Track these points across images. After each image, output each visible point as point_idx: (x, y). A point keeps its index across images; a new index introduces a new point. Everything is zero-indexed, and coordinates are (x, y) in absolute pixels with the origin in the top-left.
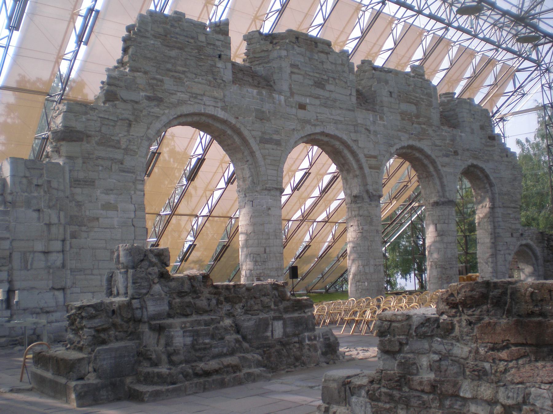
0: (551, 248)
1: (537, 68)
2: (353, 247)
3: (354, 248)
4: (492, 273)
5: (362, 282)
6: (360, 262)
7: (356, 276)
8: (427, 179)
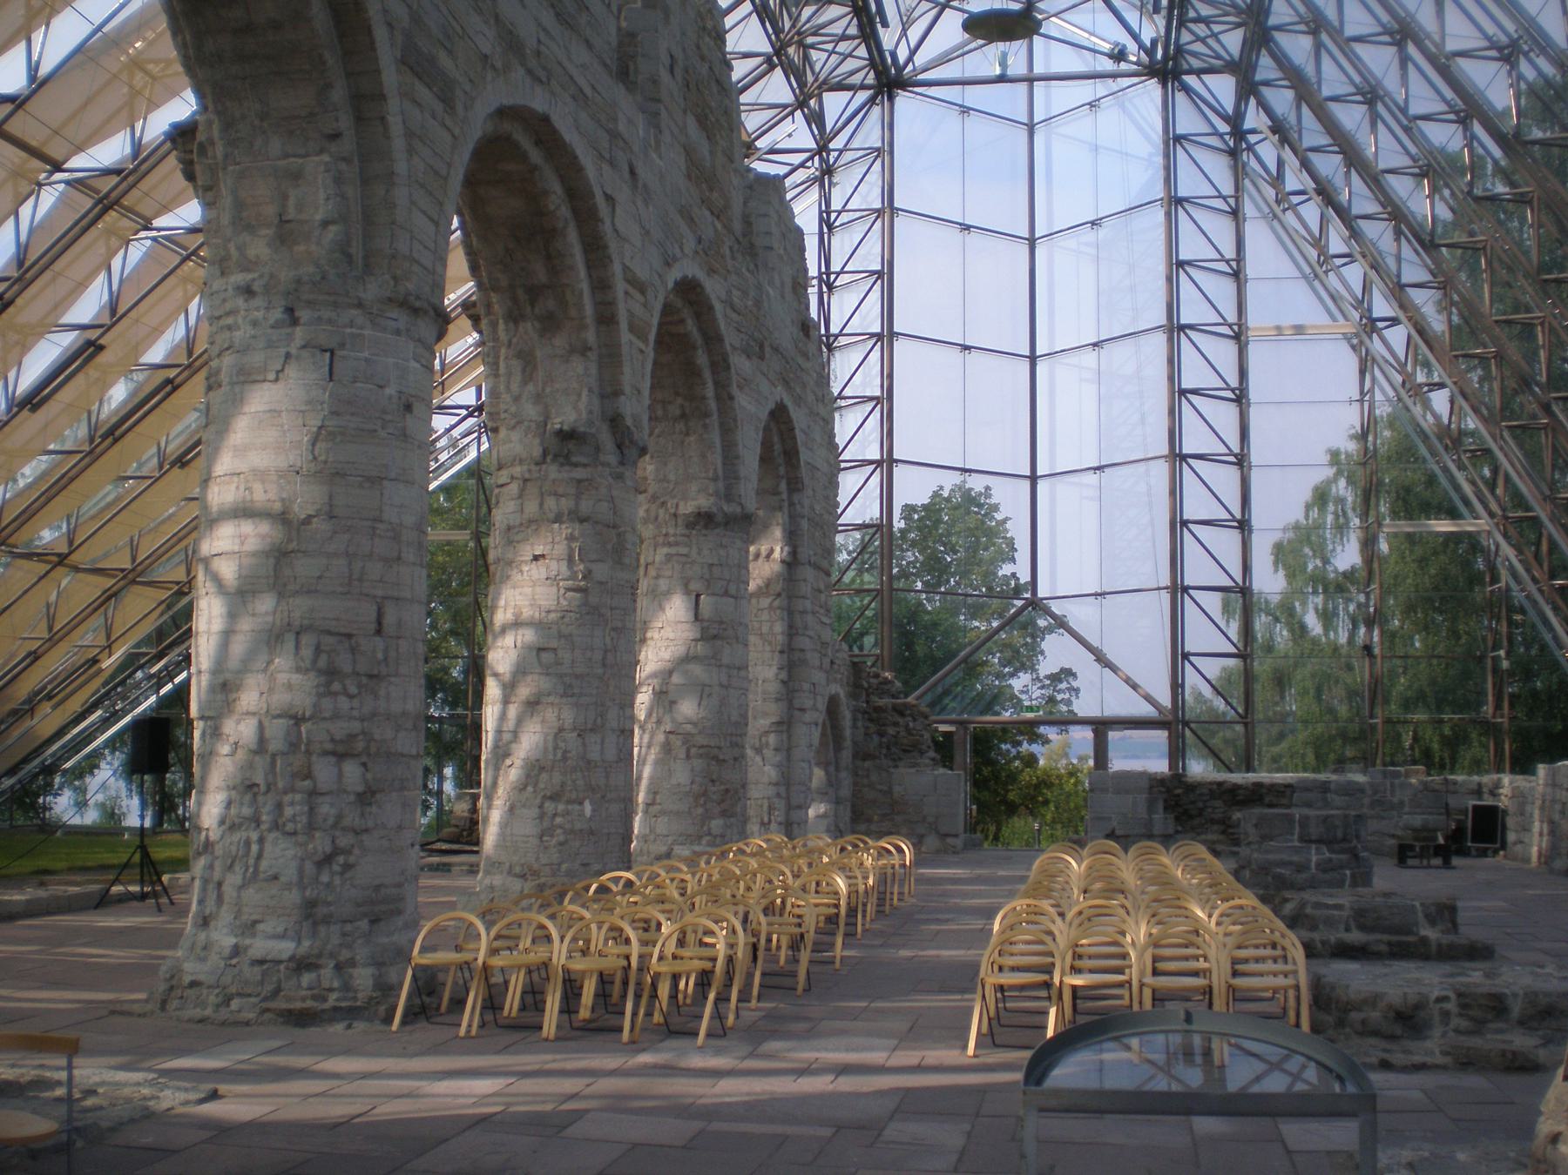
0: (875, 715)
2: (540, 650)
3: (544, 655)
4: (776, 784)
5: (569, 802)
6: (568, 716)
7: (544, 776)
8: (680, 426)
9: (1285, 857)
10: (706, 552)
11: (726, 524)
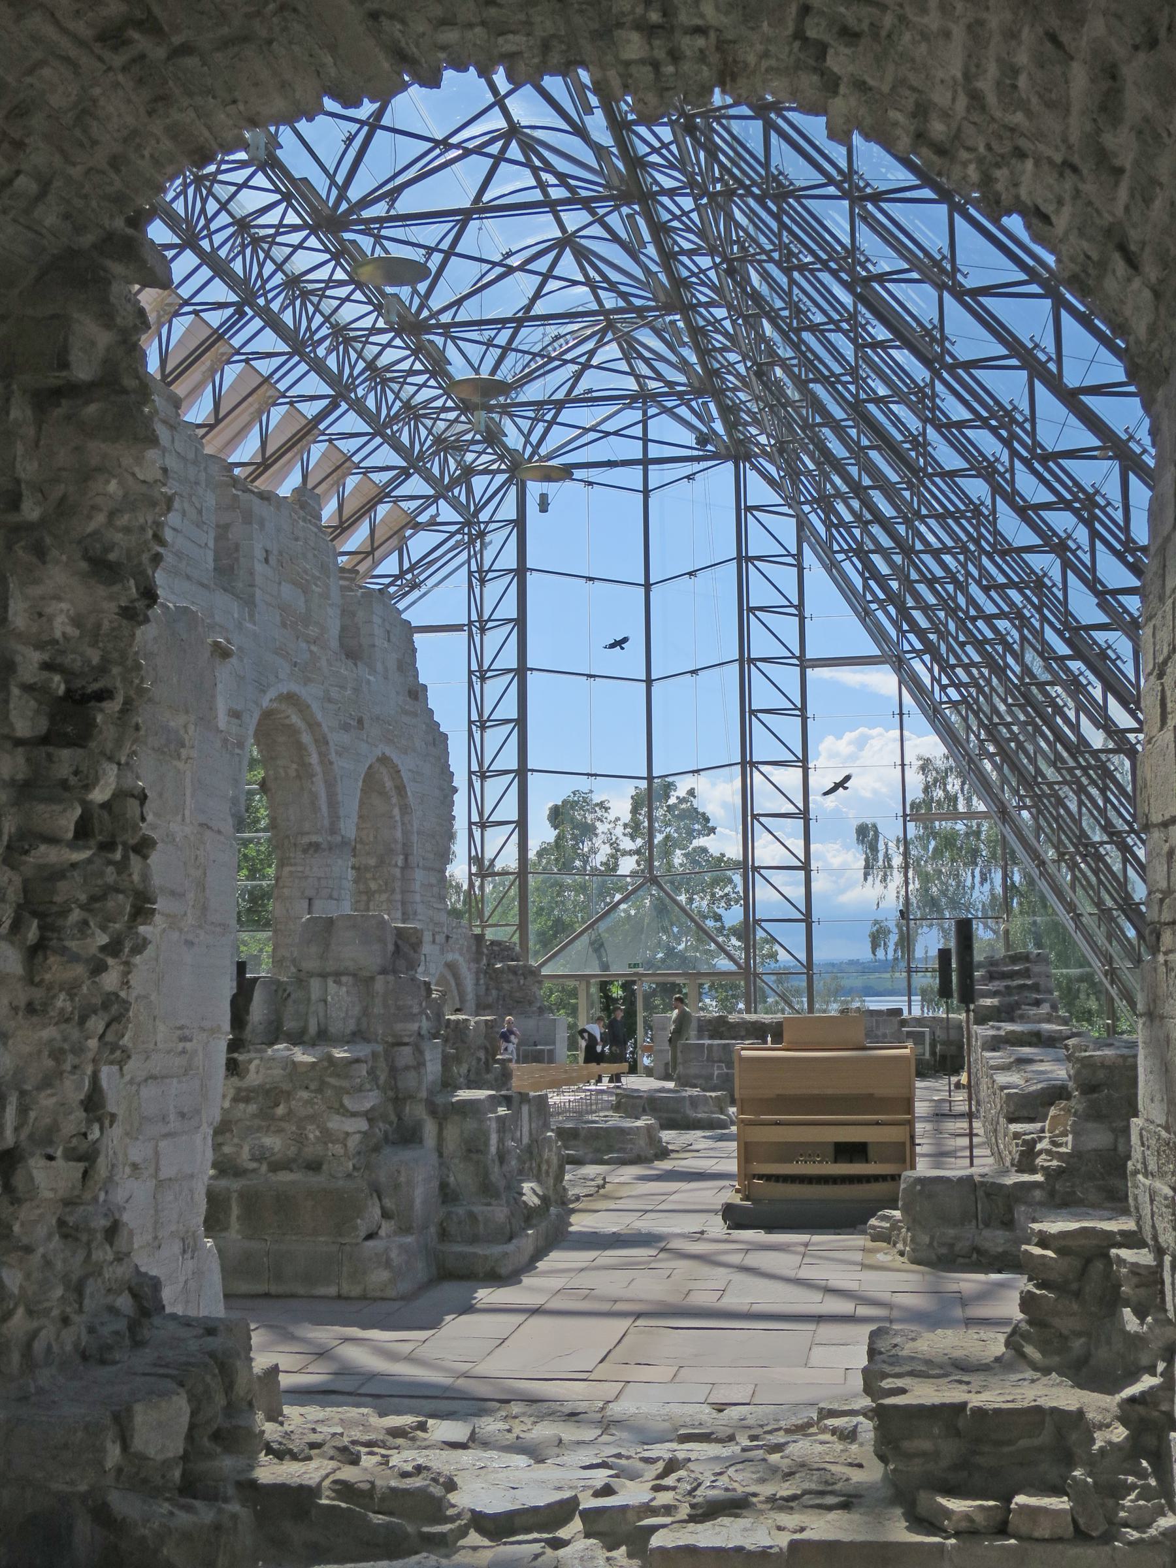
1: (462, 529)
11: (330, 849)
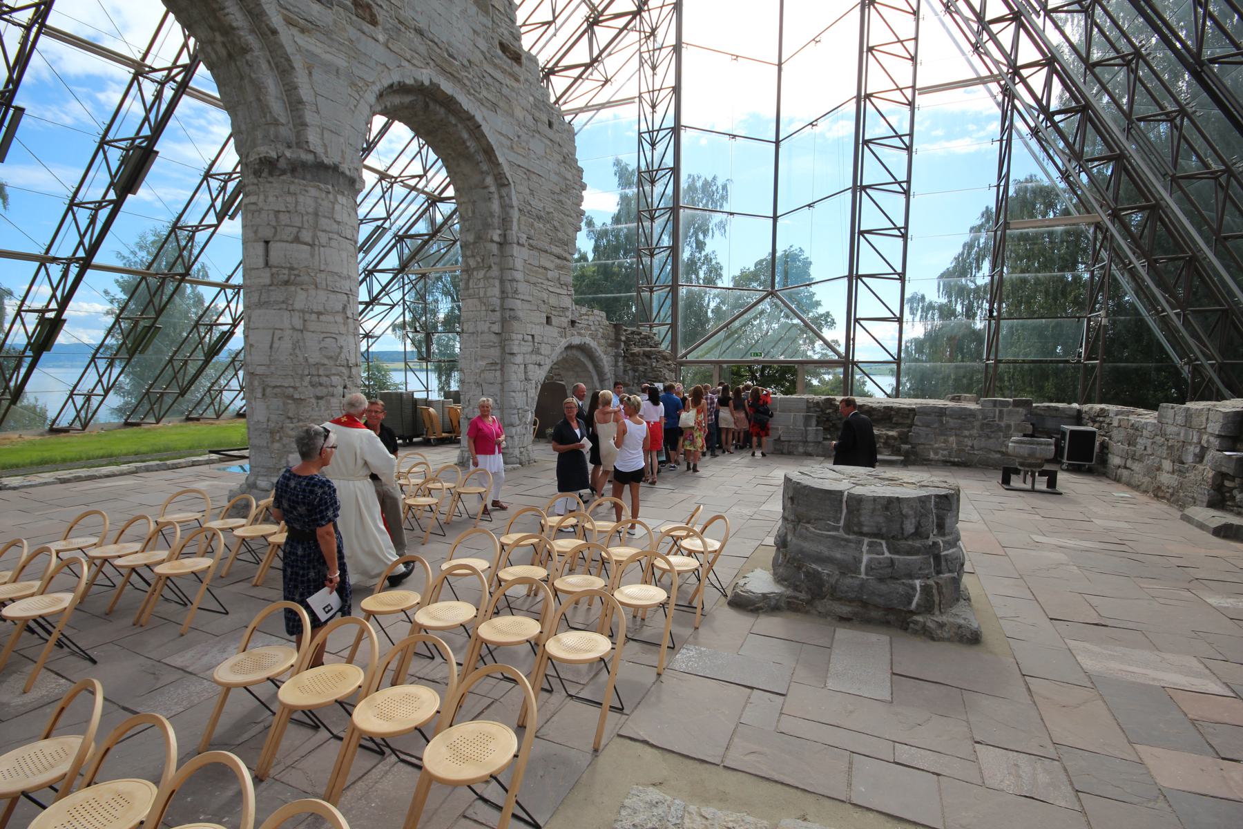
0: (631, 358)
9: (823, 550)
10: (271, 199)
